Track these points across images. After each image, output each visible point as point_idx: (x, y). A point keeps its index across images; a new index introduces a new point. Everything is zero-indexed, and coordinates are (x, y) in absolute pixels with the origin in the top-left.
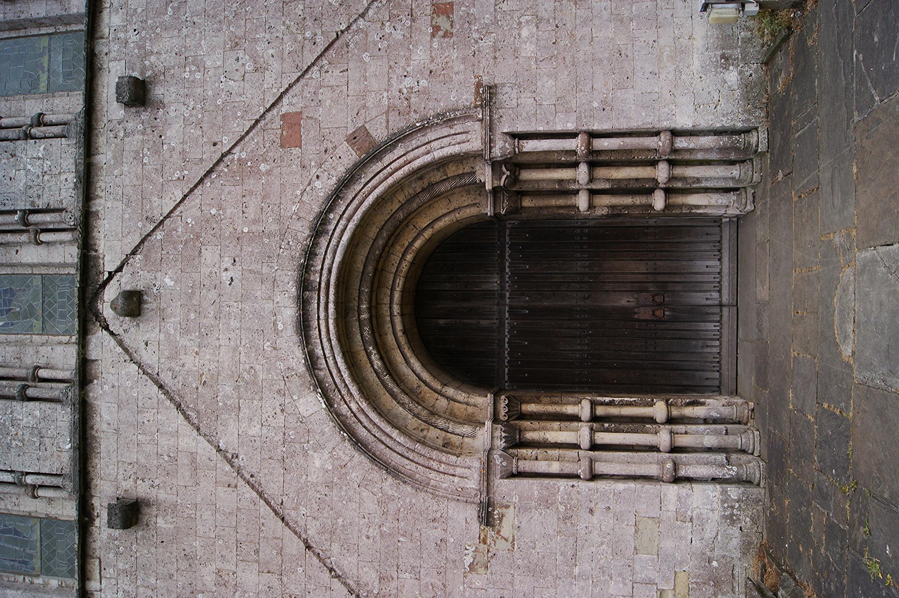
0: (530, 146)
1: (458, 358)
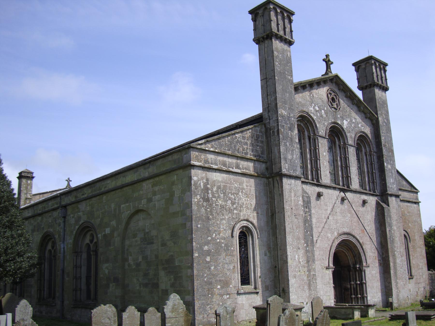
0: (43, 292)
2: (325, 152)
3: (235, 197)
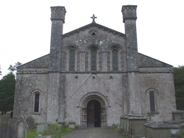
0: (106, 110)
1: (89, 104)
2: (83, 58)
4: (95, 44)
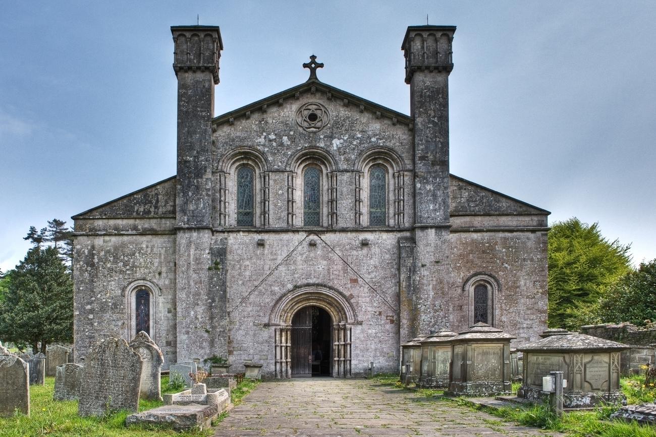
3: (129, 259)
4: (317, 148)
